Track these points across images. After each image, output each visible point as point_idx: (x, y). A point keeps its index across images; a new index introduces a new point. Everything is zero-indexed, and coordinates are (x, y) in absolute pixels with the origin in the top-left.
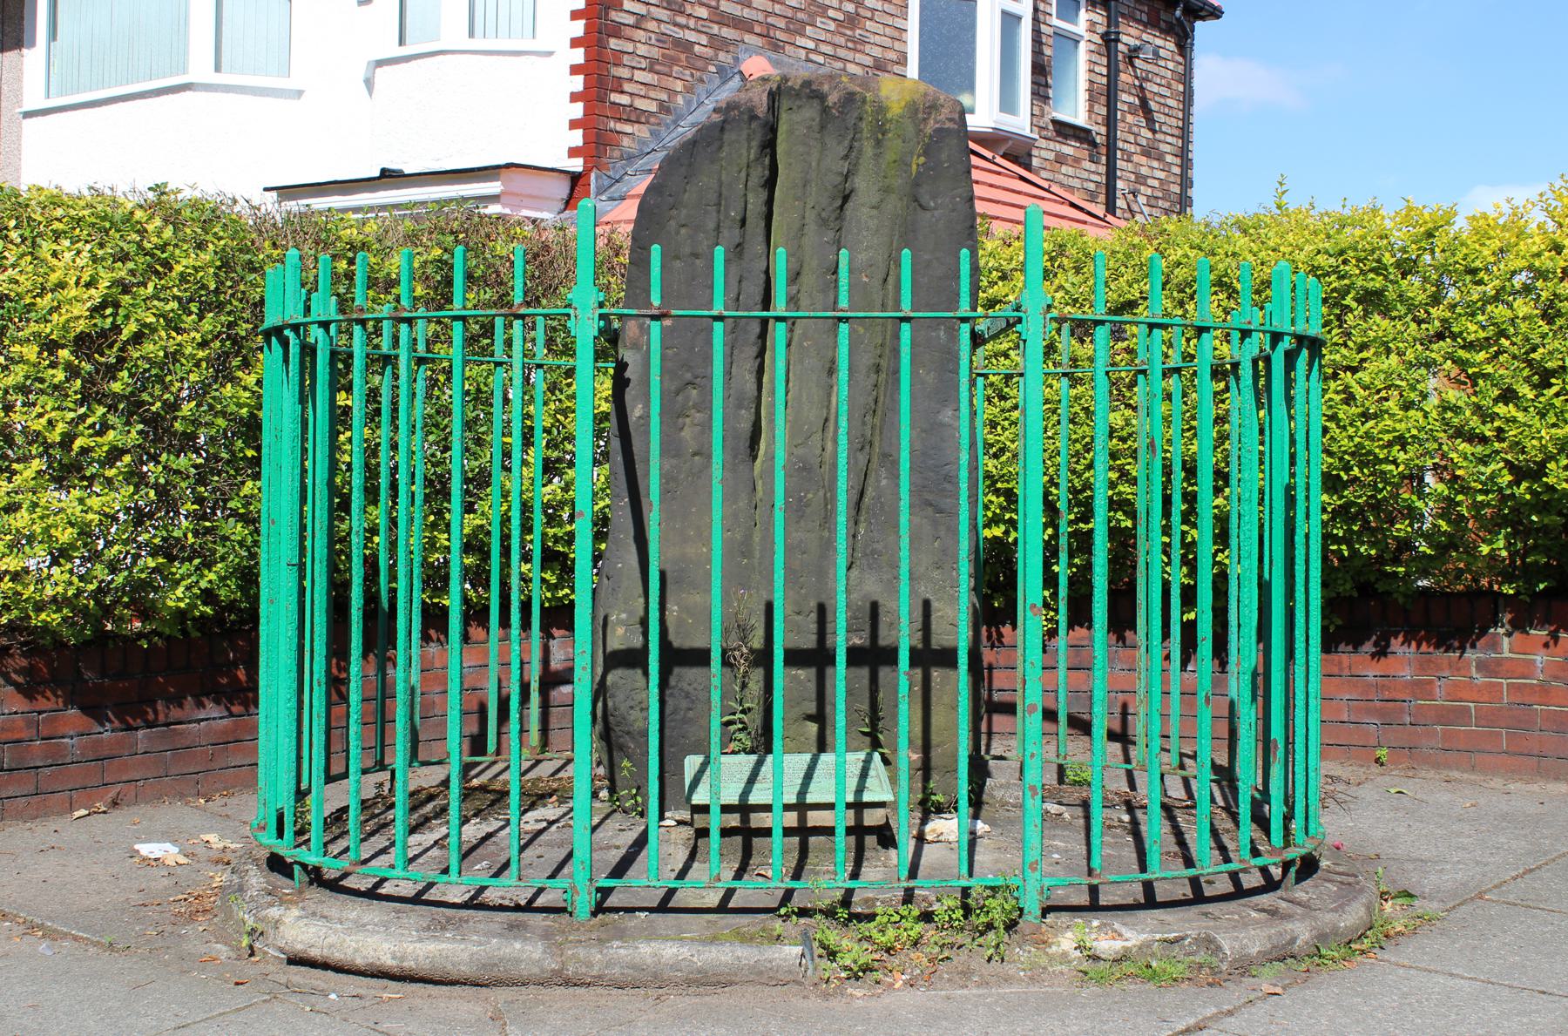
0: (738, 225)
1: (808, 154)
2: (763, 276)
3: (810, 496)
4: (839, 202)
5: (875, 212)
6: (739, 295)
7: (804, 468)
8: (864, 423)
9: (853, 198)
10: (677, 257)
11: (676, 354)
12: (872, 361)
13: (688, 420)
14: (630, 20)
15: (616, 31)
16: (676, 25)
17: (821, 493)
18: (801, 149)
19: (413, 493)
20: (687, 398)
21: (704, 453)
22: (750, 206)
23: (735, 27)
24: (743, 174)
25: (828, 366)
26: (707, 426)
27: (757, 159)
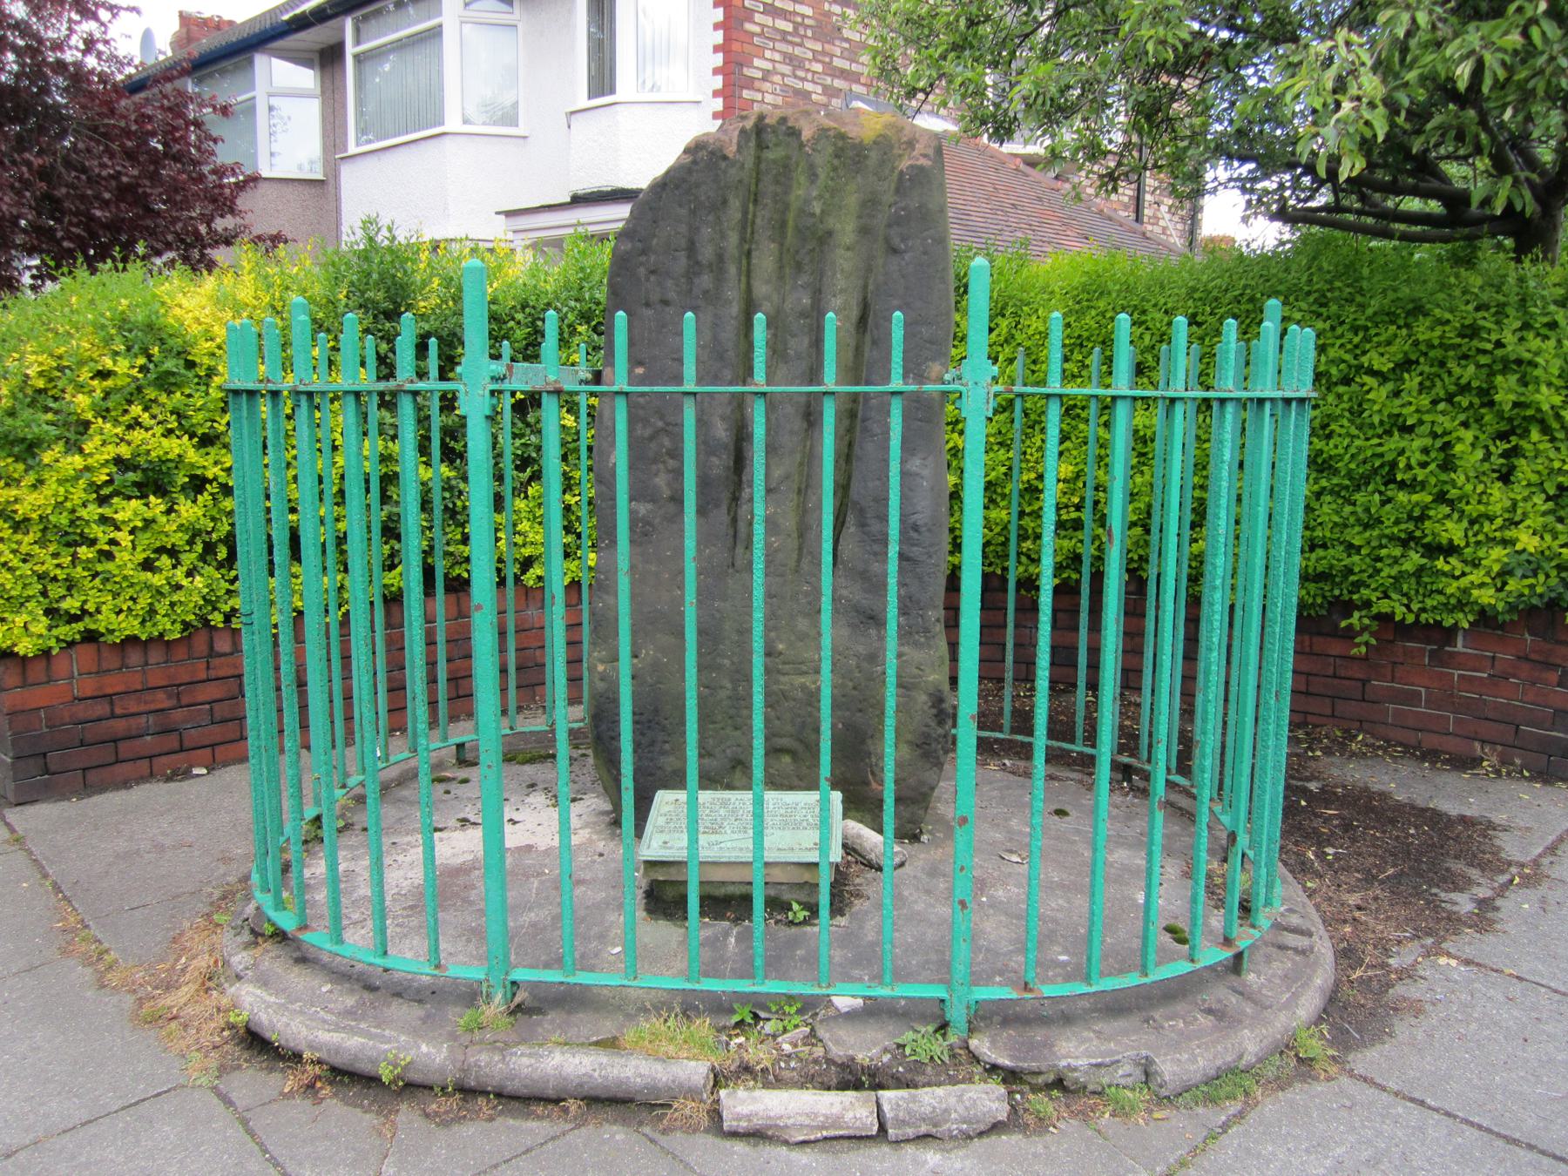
14: (759, 75)
15: (750, 83)
16: (796, 77)
19: (327, 624)
21: (677, 499)
23: (845, 79)
26: (678, 473)
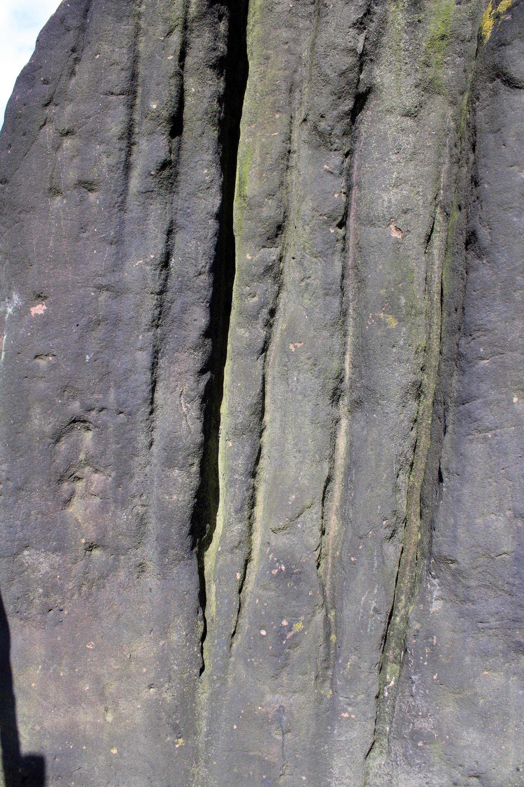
0: (164, 129)
1: (296, 41)
2: (213, 225)
3: (298, 627)
4: (348, 104)
5: (409, 122)
6: (168, 256)
7: (289, 574)
8: (396, 489)
9: (372, 102)
10: (55, 191)
11: (53, 367)
12: (412, 377)
13: (80, 485)
17: (319, 617)
18: (285, 34)
20: (76, 448)
22: (189, 101)
24: (176, 38)
25: (331, 385)
27: (202, 16)
